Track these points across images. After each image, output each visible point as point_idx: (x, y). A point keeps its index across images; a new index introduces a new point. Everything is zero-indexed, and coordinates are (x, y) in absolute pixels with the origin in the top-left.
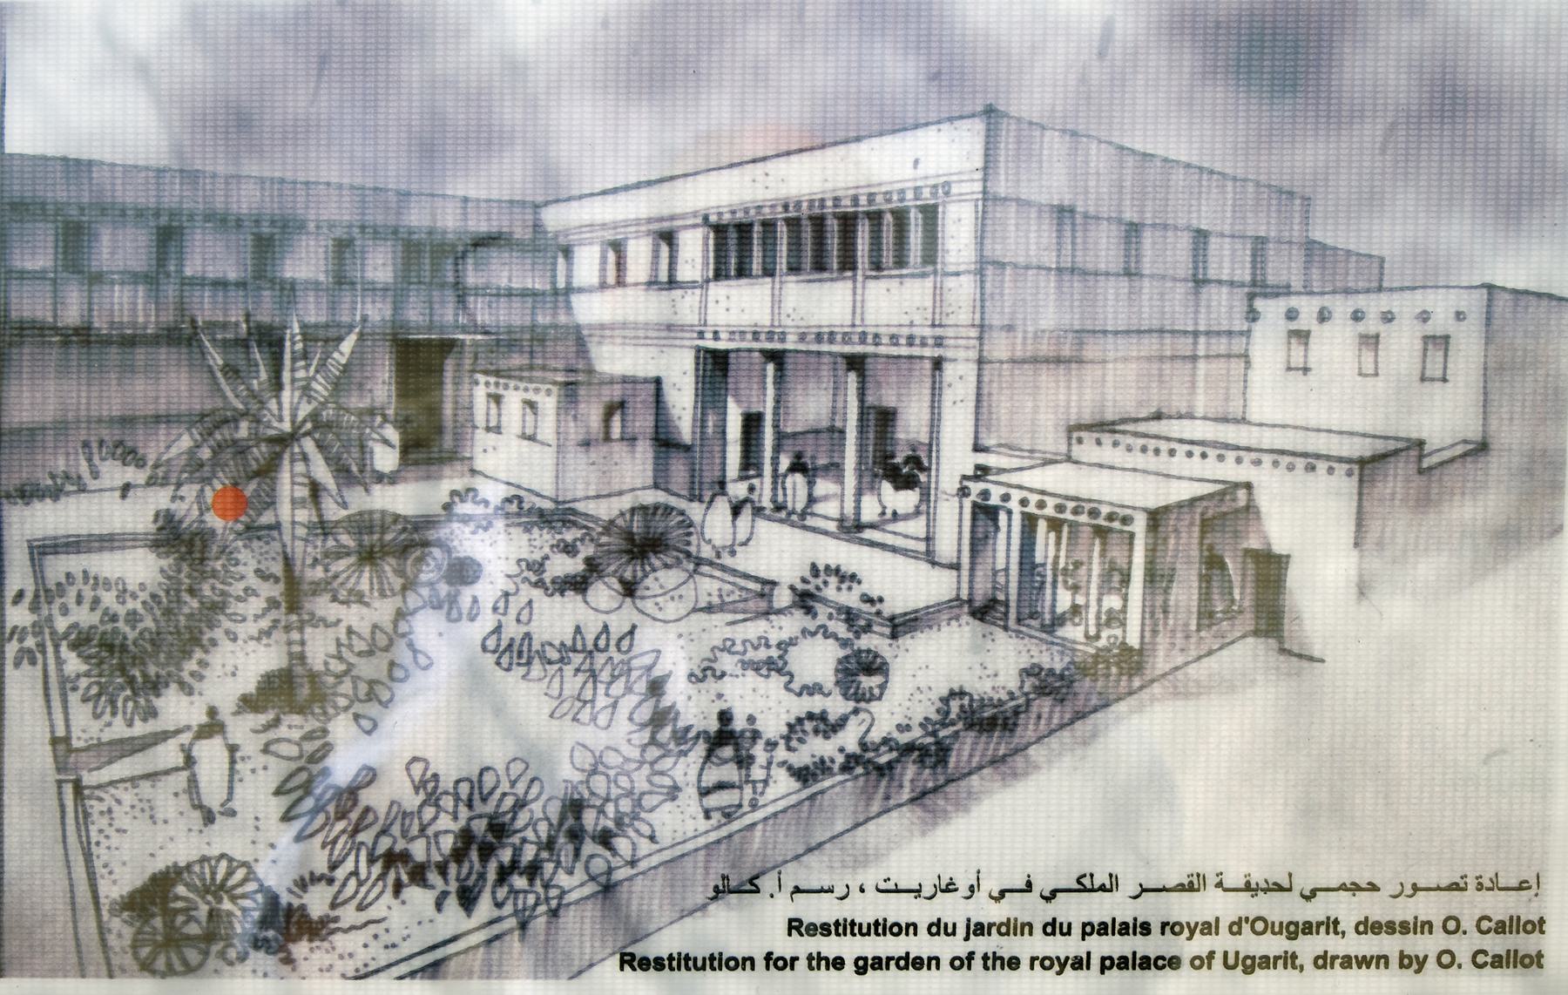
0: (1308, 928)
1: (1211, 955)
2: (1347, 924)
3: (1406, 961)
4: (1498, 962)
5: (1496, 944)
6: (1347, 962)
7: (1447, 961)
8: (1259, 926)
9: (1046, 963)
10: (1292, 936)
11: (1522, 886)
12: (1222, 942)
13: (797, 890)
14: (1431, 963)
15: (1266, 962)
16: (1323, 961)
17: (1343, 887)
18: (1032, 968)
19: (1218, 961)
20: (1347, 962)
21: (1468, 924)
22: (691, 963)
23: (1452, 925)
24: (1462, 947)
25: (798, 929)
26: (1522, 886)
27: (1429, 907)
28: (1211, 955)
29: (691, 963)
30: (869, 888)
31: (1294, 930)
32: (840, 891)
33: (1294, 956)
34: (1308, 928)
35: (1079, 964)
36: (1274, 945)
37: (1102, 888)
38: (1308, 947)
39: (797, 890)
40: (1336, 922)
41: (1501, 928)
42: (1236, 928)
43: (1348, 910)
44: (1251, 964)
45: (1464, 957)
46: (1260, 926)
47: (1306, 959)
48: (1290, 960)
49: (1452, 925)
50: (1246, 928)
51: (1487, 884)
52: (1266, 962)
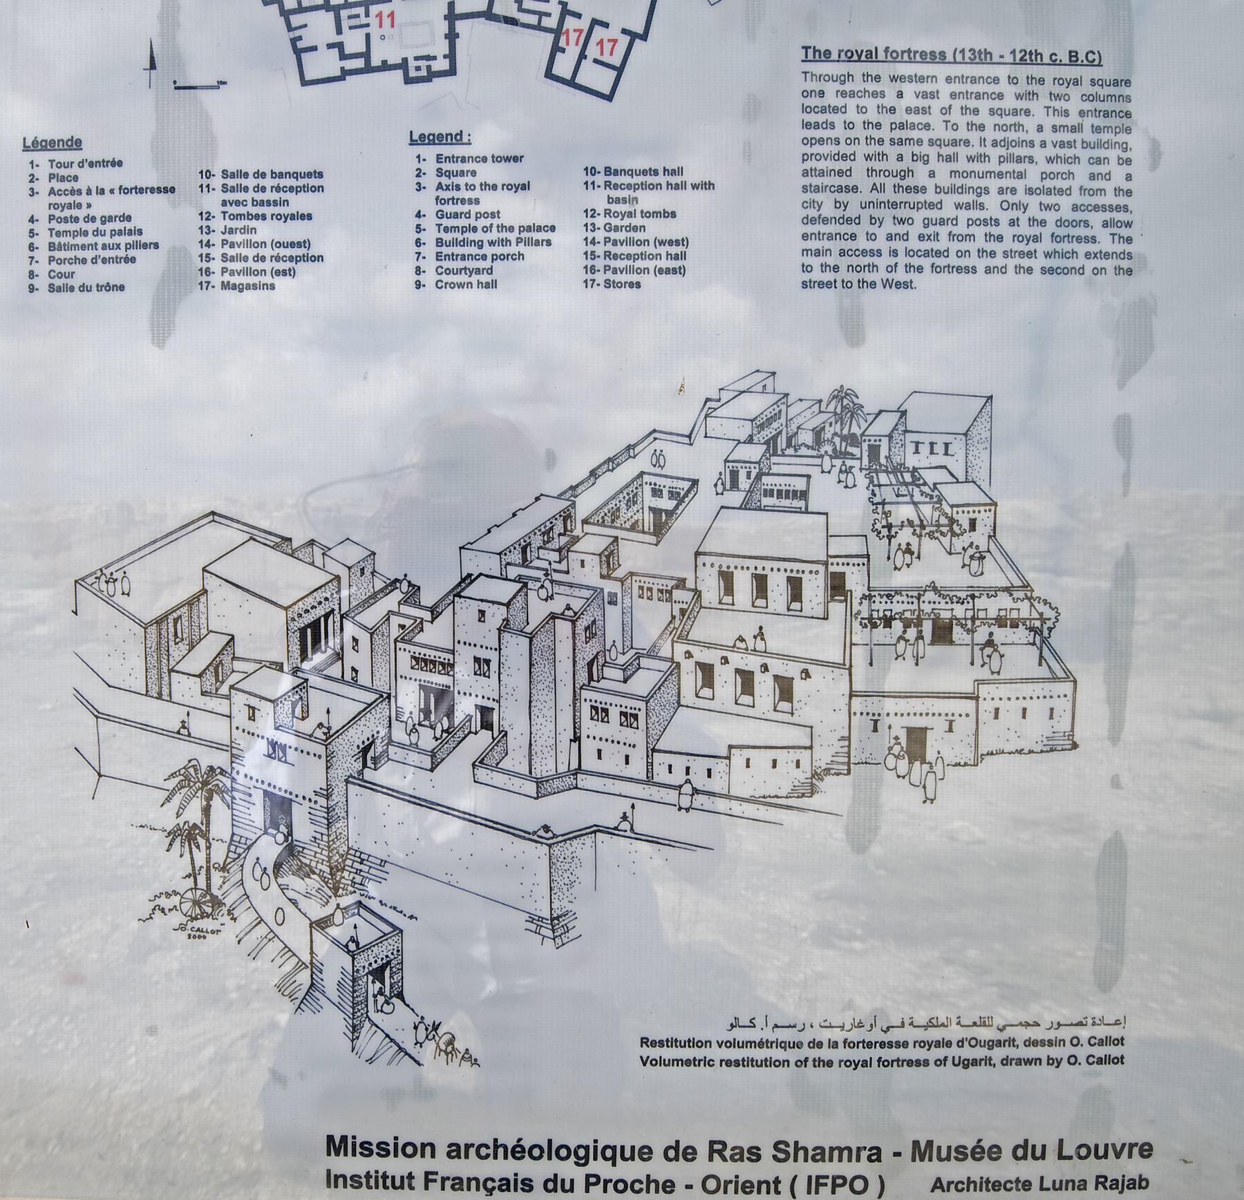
0: (999, 1043)
1: (946, 1059)
2: (1019, 1042)
3: (1051, 1061)
4: (1100, 1061)
5: (1100, 1052)
6: (1019, 1062)
7: (1073, 1060)
8: (973, 1043)
9: (847, 1063)
10: (991, 1048)
11: (1117, 1023)
12: (954, 1051)
13: (776, 1026)
14: (1064, 1063)
15: (975, 1062)
16: (1006, 1062)
17: (1021, 1024)
18: (1044, 1147)
19: (949, 1062)
20: (1019, 1062)
21: (1084, 1041)
22: (389, 1182)
23: (1075, 1041)
24: (1082, 1052)
25: (720, 1152)
26: (1117, 1023)
27: (1065, 1033)
28: (946, 1059)
29: (389, 1182)
30: (816, 1025)
31: (992, 1044)
32: (800, 1027)
33: (990, 1059)
34: (999, 1043)
35: (865, 1064)
36: (980, 1053)
37: (943, 1025)
38: (998, 1054)
39: (776, 1026)
40: (1014, 1040)
41: (1101, 1043)
42: (961, 1043)
43: (1022, 1034)
44: (966, 1064)
45: (1082, 1059)
46: (975, 1043)
47: (996, 1060)
48: (988, 1061)
49: (1075, 1042)
50: (966, 1044)
51: (1098, 1022)
52: (975, 1062)
